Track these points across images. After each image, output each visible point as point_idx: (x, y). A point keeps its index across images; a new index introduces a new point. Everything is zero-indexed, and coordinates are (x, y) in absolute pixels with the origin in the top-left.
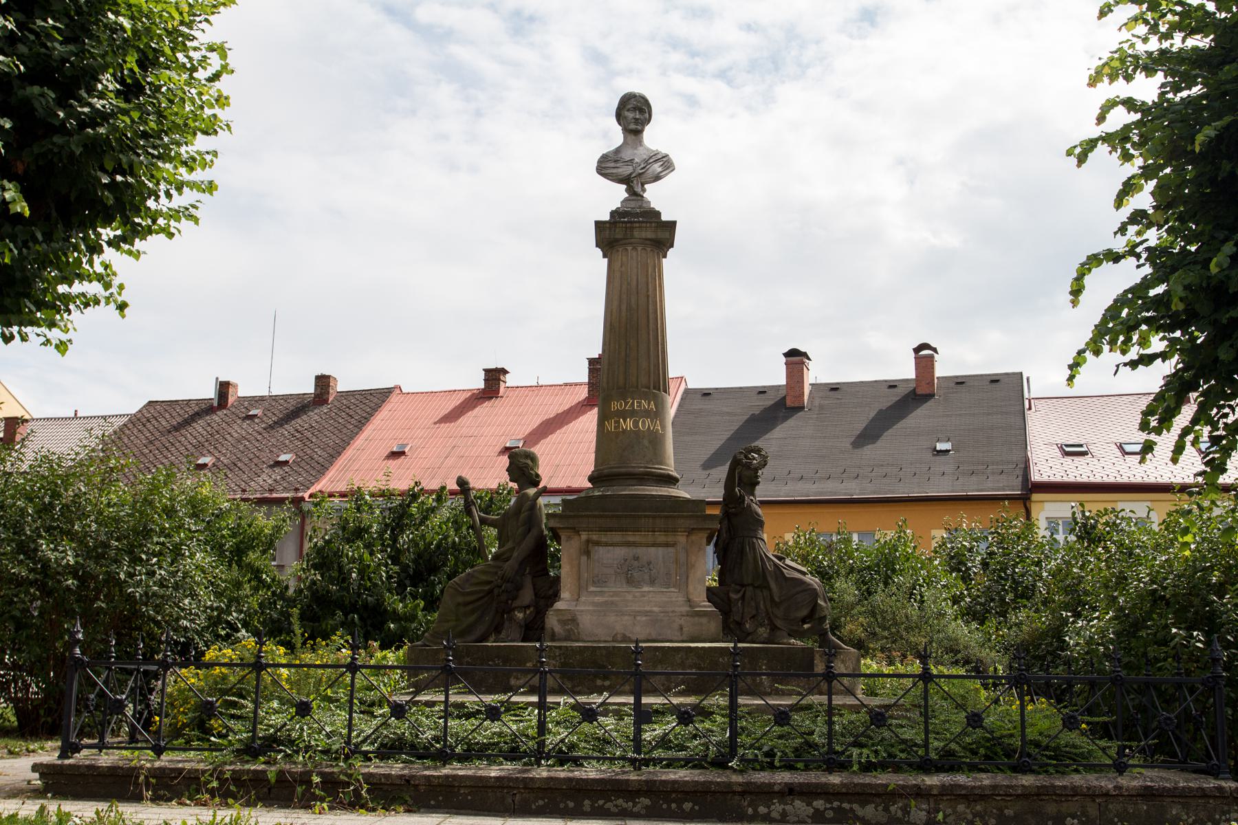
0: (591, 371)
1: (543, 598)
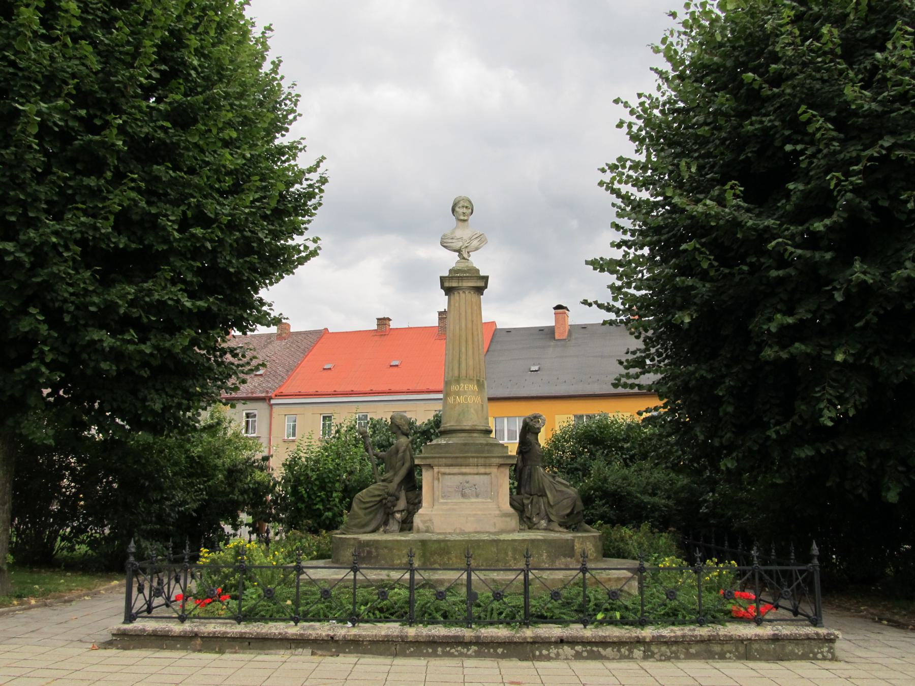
0: (440, 319)
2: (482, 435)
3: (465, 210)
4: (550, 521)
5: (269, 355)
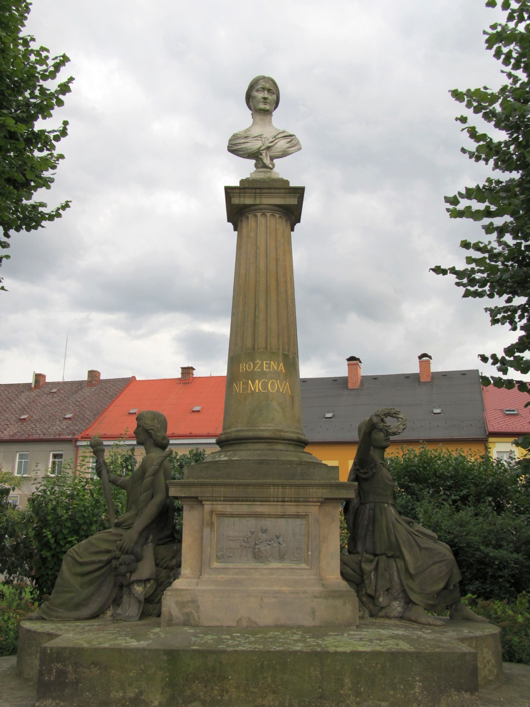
1: (165, 568)
2: (291, 448)
3: (266, 94)
4: (409, 602)
5: (79, 400)
